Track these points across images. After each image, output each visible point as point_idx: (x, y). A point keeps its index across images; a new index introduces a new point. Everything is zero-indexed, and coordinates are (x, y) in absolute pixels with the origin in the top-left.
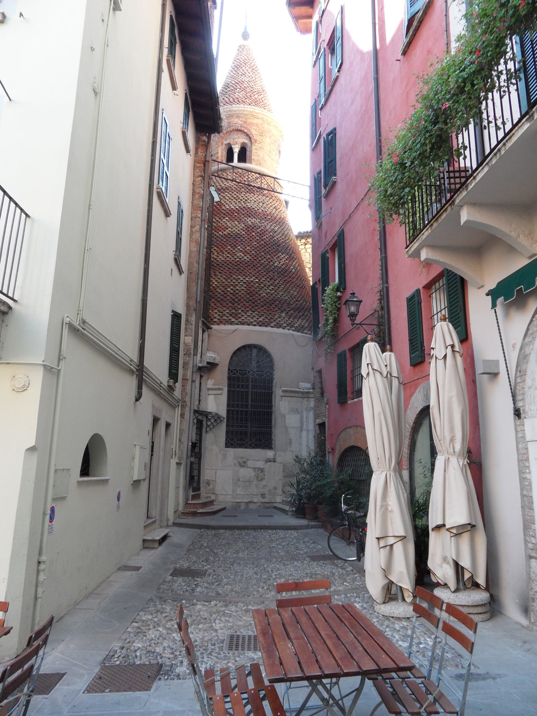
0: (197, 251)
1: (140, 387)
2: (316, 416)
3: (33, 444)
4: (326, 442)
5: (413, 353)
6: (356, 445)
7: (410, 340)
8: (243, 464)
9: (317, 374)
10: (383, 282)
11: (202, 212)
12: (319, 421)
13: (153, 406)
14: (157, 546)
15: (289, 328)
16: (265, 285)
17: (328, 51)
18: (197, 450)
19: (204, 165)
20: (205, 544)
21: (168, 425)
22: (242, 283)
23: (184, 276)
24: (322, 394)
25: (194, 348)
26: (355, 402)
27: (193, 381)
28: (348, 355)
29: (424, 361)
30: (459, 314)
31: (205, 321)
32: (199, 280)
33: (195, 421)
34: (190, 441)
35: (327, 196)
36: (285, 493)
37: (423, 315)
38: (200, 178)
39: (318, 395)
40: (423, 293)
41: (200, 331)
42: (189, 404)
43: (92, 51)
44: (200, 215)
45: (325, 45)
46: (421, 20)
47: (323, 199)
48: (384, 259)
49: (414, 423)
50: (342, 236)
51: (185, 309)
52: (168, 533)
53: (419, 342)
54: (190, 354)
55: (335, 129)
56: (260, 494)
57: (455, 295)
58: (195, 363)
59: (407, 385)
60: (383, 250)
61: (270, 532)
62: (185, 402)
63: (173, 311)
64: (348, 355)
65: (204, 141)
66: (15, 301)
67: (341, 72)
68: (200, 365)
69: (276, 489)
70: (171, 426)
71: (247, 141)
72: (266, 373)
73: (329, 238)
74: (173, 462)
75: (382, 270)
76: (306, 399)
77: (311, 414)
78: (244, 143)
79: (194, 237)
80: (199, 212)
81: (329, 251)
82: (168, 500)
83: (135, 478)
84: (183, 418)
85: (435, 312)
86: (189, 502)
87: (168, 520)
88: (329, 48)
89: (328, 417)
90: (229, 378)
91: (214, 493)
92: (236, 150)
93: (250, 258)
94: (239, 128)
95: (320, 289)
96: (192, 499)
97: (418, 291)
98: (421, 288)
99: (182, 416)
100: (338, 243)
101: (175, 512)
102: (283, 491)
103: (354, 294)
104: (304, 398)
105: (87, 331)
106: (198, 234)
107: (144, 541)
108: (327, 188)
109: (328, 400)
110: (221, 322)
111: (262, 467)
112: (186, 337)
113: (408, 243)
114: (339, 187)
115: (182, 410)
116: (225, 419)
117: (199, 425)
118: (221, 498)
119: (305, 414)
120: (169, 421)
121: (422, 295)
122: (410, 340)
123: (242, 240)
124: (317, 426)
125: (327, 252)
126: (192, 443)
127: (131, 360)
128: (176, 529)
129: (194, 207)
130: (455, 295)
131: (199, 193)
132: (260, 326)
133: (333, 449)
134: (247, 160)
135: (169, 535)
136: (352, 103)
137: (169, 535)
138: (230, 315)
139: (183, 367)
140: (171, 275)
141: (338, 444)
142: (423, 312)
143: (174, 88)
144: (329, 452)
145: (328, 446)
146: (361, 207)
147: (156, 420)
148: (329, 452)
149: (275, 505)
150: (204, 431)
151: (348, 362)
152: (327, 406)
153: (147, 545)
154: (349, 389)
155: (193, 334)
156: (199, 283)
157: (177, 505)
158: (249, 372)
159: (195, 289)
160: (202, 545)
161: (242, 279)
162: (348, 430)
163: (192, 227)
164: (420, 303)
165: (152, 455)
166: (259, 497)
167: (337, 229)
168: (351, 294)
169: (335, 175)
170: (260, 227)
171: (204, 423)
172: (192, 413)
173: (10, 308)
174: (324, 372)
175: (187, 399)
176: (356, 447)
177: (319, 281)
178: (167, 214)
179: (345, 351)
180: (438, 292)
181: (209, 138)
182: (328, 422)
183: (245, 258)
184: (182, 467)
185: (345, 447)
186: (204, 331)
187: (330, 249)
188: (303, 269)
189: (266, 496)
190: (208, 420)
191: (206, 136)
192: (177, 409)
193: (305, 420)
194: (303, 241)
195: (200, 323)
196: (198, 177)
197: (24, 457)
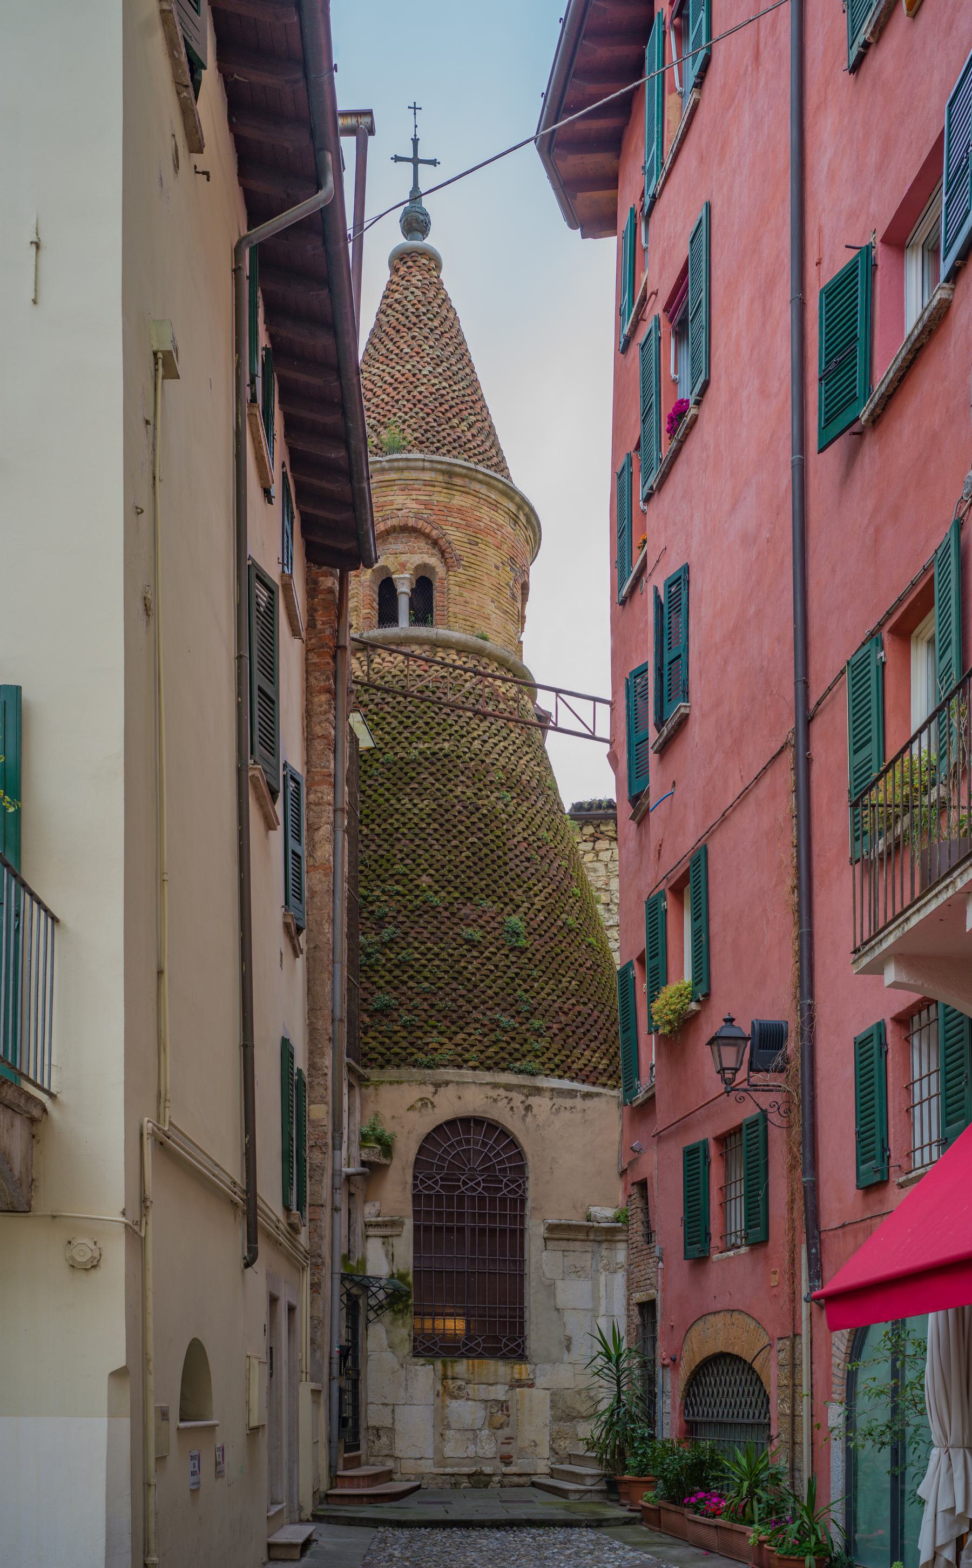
1: (252, 1239)
2: (632, 1286)
3: (124, 1364)
5: (864, 1162)
6: (729, 1351)
8: (456, 1392)
9: (635, 1191)
10: (801, 993)
11: (334, 786)
12: (639, 1297)
14: (298, 1557)
15: (561, 1073)
16: (496, 966)
17: (666, 329)
19: (334, 658)
20: (397, 1553)
21: (291, 1309)
22: (437, 962)
24: (649, 1236)
25: (334, 1130)
26: (729, 1258)
27: (335, 1209)
28: (713, 1151)
29: (887, 1181)
30: (963, 1091)
32: (338, 966)
35: (664, 749)
36: (557, 1453)
37: (890, 1080)
38: (324, 697)
39: (638, 1238)
40: (892, 1032)
42: (328, 1260)
43: (138, 513)
45: (656, 308)
46: (918, 345)
47: (653, 758)
48: (805, 938)
50: (702, 862)
52: (311, 1535)
53: (877, 1138)
54: (326, 1145)
55: (686, 569)
56: (498, 1456)
57: (958, 1059)
58: (337, 1168)
59: (849, 1228)
60: (804, 917)
61: (533, 1531)
62: (320, 1256)
64: (713, 1151)
65: (330, 591)
66: (52, 1096)
69: (536, 1445)
70: (297, 1311)
71: (434, 561)
72: (507, 1186)
73: (669, 861)
74: (305, 1390)
75: (800, 961)
76: (604, 1245)
77: (620, 1279)
78: (425, 566)
81: (668, 895)
82: (298, 1468)
83: (254, 1423)
84: (317, 1292)
85: (917, 1077)
86: (340, 1473)
87: (301, 1508)
88: (671, 320)
89: (664, 1290)
90: (416, 1198)
91: (392, 1456)
92: (404, 588)
94: (411, 522)
95: (642, 988)
96: (345, 1469)
97: (881, 1025)
99: (315, 1287)
100: (692, 874)
101: (314, 1493)
102: (552, 1449)
103: (732, 1020)
104: (600, 1242)
105: (173, 1141)
107: (270, 1546)
108: (665, 730)
109: (662, 1251)
111: (503, 1398)
113: (858, 944)
114: (696, 732)
117: (352, 1308)
118: (408, 1467)
119: (602, 1279)
121: (889, 1035)
122: (858, 1133)
123: (431, 846)
124: (636, 1309)
125: (662, 895)
126: (341, 1347)
127: (234, 1183)
128: (323, 1527)
130: (958, 1059)
131: (323, 737)
132: (489, 1069)
133: (674, 1360)
135: (314, 1537)
136: (734, 508)
137: (314, 1537)
140: (281, 966)
141: (686, 1348)
142: (890, 1075)
144: (664, 1366)
145: (662, 1352)
146: (751, 798)
147: (273, 1300)
148: (664, 1366)
149: (535, 1479)
150: (362, 1320)
151: (713, 1165)
152: (661, 1265)
153: (276, 1553)
154: (715, 1227)
155: (329, 1099)
156: (338, 973)
157: (317, 1479)
158: (465, 1183)
159: (328, 988)
160: (391, 1555)
161: (436, 949)
164: (883, 1053)
165: (271, 1375)
166: (497, 1462)
167: (687, 843)
168: (725, 1020)
169: (686, 695)
170: (478, 809)
173: (45, 1110)
175: (325, 1250)
176: (729, 1354)
177: (641, 959)
179: (705, 1142)
180: (925, 1031)
181: (343, 582)
182: (663, 1300)
184: (324, 1396)
185: (705, 1355)
186: (351, 1086)
187: (670, 889)
188: (590, 920)
189: (514, 1459)
193: (602, 1293)
194: (589, 830)
196: (320, 692)
197: (109, 1388)
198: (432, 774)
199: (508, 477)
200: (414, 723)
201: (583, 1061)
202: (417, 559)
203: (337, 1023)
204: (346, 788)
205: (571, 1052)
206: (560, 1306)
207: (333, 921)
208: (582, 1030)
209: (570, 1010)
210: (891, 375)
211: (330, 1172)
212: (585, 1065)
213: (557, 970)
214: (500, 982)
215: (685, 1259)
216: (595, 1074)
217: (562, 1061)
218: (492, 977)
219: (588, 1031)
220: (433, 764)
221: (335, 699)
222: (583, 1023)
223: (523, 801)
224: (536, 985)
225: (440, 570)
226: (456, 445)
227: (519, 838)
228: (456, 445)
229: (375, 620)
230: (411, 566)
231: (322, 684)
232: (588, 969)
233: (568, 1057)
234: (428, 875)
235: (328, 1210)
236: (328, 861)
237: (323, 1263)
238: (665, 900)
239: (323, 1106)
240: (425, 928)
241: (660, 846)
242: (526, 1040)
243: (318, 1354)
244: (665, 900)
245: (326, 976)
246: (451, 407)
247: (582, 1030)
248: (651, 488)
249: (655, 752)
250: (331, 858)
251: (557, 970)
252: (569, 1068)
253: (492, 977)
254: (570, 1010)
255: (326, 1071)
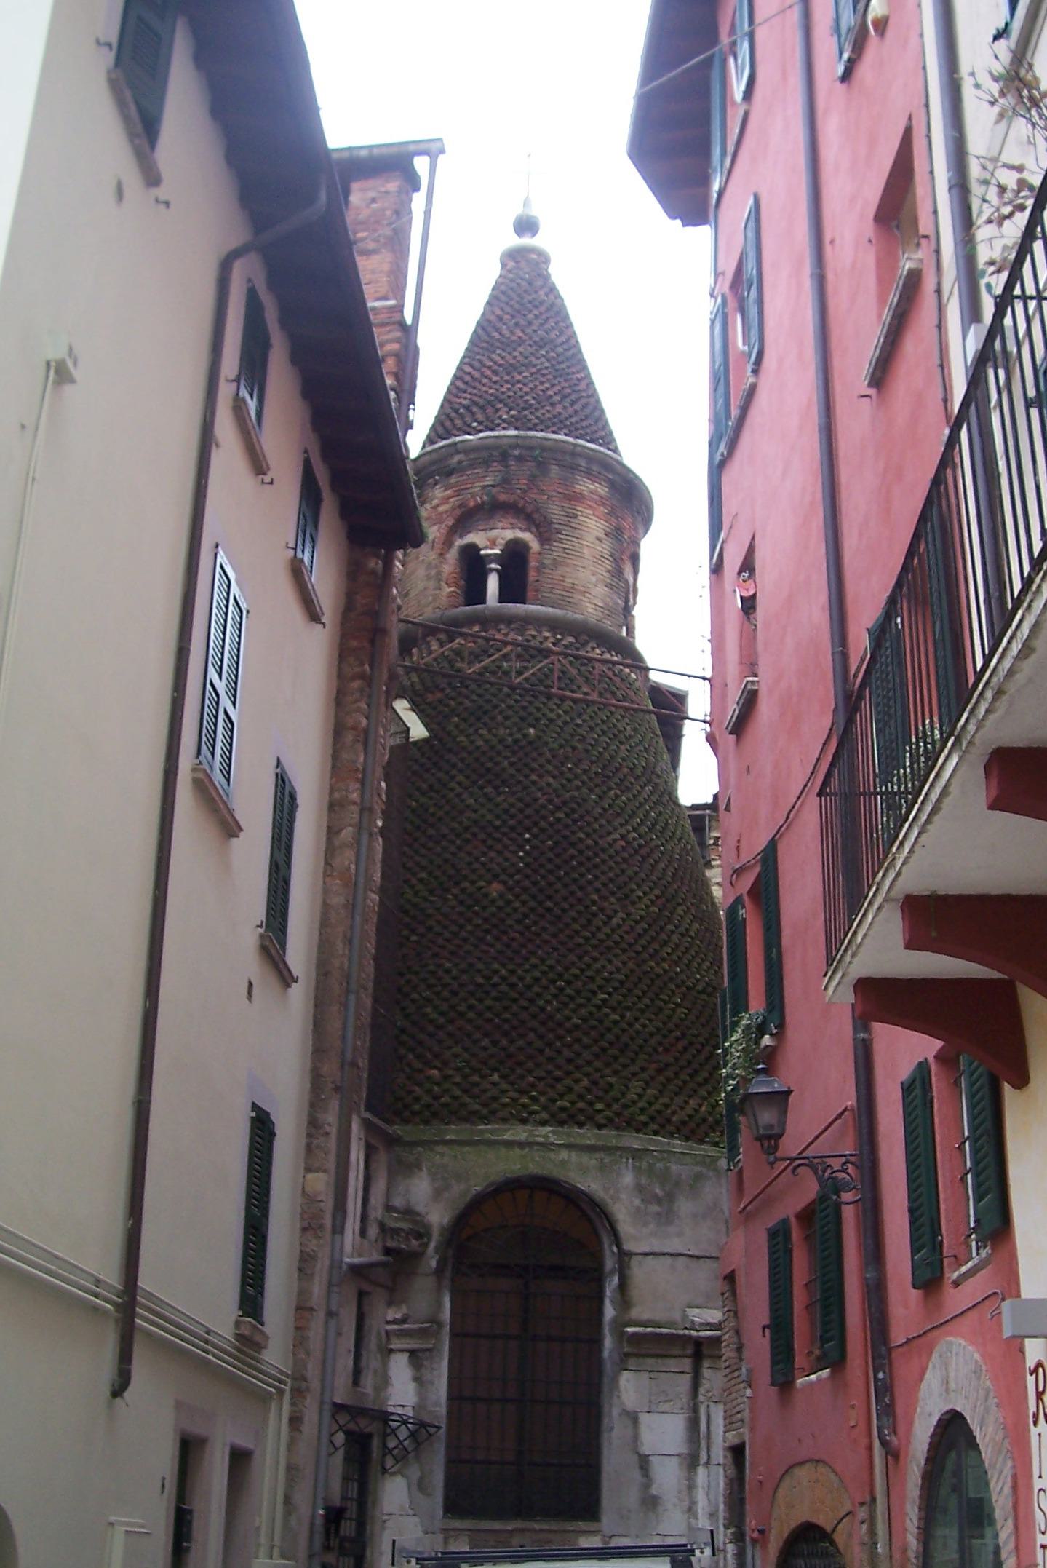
0: (345, 906)
1: (125, 1357)
4: (748, 1507)
7: (911, 1211)
11: (363, 784)
13: (179, 1405)
18: (348, 1528)
19: (372, 642)
21: (240, 1459)
23: (299, 995)
26: (811, 1383)
27: (330, 1314)
28: (796, 1235)
31: (376, 1120)
33: (340, 1438)
34: (320, 1502)
38: (356, 684)
41: (357, 1155)
44: (355, 796)
49: (928, 1460)
51: (309, 1085)
54: (321, 1227)
58: (337, 1256)
63: (255, 1107)
65: (373, 572)
67: (763, 375)
68: (357, 1260)
79: (337, 862)
80: (355, 786)
89: (752, 1429)
93: (532, 904)
98: (931, 1060)
99: (295, 1421)
106: (350, 854)
110: (435, 1115)
112: (310, 1176)
115: (293, 1404)
116: (443, 1431)
120: (244, 1442)
122: (911, 1211)
126: (327, 1509)
127: (98, 1282)
129: (338, 768)
131: (354, 728)
133: (761, 1532)
134: (530, 594)
138: (465, 1091)
139: (300, 1270)
143: (258, 466)
155: (331, 1164)
162: (797, 1471)
163: (332, 832)
171: (375, 1443)
172: (327, 1415)
174: (741, 1279)
175: (312, 1371)
178: (229, 828)
179: (785, 1222)
181: (388, 565)
183: (517, 904)
185: (793, 1524)
186: (370, 1151)
187: (749, 892)
190: (387, 1432)
191: (378, 556)
192: (274, 1406)
195: (356, 1126)
198: (512, 764)
199: (615, 450)
200: (496, 707)
201: (689, 1110)
202: (509, 534)
203: (346, 1067)
204: (383, 784)
205: (672, 1099)
206: (646, 1449)
207: (350, 942)
208: (689, 1071)
209: (672, 1045)
210: (882, 340)
211: (327, 1263)
212: (690, 1117)
213: (657, 995)
214: (583, 1011)
215: (773, 1384)
216: (704, 1128)
217: (659, 1112)
218: (572, 1006)
219: (696, 1071)
220: (514, 753)
221: (370, 686)
222: (689, 1062)
223: (622, 791)
224: (628, 1014)
225: (535, 545)
226: (556, 420)
227: (616, 836)
228: (556, 420)
229: (461, 600)
230: (501, 542)
231: (357, 670)
232: (699, 992)
233: (667, 1106)
234: (499, 882)
235: (321, 1315)
236: (348, 869)
237: (308, 1389)
238: (744, 907)
239: (321, 1175)
240: (492, 946)
241: (739, 841)
242: (611, 1085)
243: (293, 1521)
244: (744, 907)
245: (335, 1008)
246: (553, 386)
247: (689, 1071)
248: (722, 455)
249: (731, 733)
250: (353, 867)
251: (657, 995)
252: (669, 1121)
253: (572, 1006)
254: (672, 1045)
255: (328, 1129)
